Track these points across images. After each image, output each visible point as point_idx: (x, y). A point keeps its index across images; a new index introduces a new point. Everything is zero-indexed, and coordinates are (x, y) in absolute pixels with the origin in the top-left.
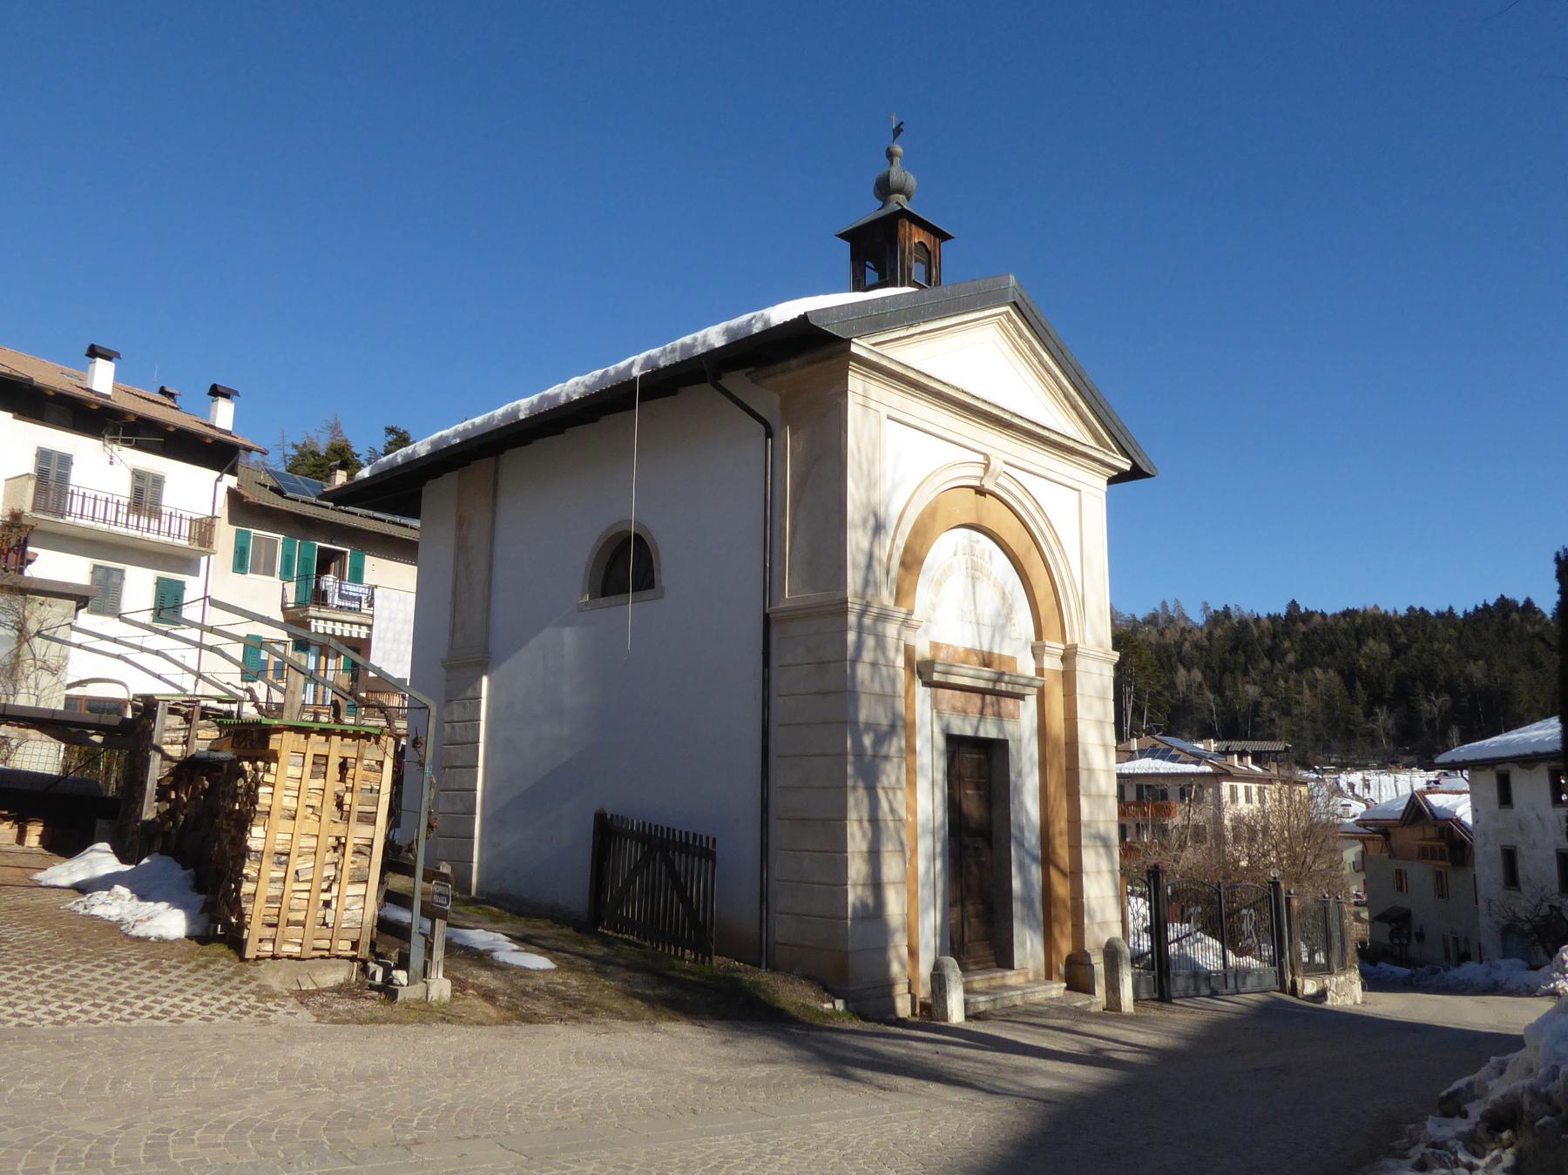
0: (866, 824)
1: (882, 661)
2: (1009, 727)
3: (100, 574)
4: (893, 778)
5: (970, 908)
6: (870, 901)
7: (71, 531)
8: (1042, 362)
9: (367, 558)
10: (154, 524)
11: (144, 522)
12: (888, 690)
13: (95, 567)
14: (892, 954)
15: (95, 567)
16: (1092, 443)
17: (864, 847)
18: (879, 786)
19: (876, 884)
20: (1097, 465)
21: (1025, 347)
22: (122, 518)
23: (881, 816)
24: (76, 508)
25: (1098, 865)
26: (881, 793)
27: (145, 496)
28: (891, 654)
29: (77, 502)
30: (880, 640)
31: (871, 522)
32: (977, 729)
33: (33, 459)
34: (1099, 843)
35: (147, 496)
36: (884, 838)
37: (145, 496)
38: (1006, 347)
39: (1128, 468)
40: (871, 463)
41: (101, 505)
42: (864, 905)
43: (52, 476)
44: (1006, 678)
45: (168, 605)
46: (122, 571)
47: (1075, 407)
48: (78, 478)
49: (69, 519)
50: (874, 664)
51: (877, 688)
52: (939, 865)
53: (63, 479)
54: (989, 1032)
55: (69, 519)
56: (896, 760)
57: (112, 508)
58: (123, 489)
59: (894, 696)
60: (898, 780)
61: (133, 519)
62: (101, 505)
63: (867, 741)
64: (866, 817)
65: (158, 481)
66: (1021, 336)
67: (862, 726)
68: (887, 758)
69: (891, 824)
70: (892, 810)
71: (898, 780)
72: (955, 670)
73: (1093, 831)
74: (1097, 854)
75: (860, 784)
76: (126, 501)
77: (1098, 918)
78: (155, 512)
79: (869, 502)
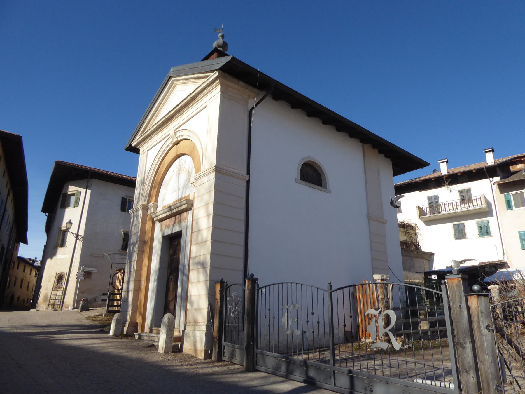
2: (184, 224)
3: (456, 227)
7: (443, 217)
8: (183, 80)
10: (471, 204)
11: (467, 205)
13: (454, 225)
14: (128, 313)
15: (454, 225)
16: (205, 80)
20: (208, 89)
21: (181, 81)
22: (459, 206)
24: (443, 209)
25: (198, 278)
27: (466, 197)
29: (443, 207)
33: (427, 201)
34: (199, 267)
35: (466, 197)
37: (466, 197)
41: (451, 205)
43: (434, 203)
44: (172, 207)
45: (484, 231)
46: (463, 224)
48: (441, 201)
49: (442, 213)
53: (437, 202)
54: (91, 335)
55: (442, 213)
57: (455, 205)
58: (457, 197)
61: (463, 206)
62: (451, 205)
65: (469, 191)
73: (196, 260)
74: (198, 272)
76: (459, 201)
77: (195, 306)
78: (470, 200)
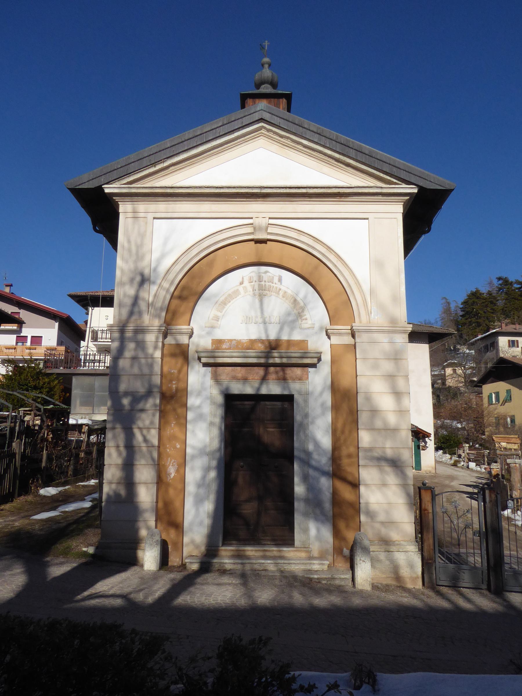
0: (122, 449)
1: (141, 355)
4: (147, 422)
5: (269, 503)
6: (123, 492)
9: (499, 337)
12: (146, 371)
14: (141, 524)
17: (120, 461)
18: (134, 426)
19: (129, 483)
20: (380, 197)
23: (135, 443)
26: (137, 432)
28: (150, 350)
30: (141, 345)
31: (138, 279)
32: (259, 389)
36: (137, 456)
38: (275, 147)
39: (415, 191)
40: (139, 247)
42: (117, 495)
47: (348, 165)
50: (134, 358)
51: (136, 370)
52: (213, 474)
56: (150, 412)
59: (151, 375)
60: (152, 423)
63: (126, 401)
64: (122, 444)
66: (282, 136)
67: (121, 394)
68: (142, 410)
69: (144, 449)
70: (145, 440)
71: (152, 423)
72: (217, 354)
75: (118, 426)
79: (136, 268)
